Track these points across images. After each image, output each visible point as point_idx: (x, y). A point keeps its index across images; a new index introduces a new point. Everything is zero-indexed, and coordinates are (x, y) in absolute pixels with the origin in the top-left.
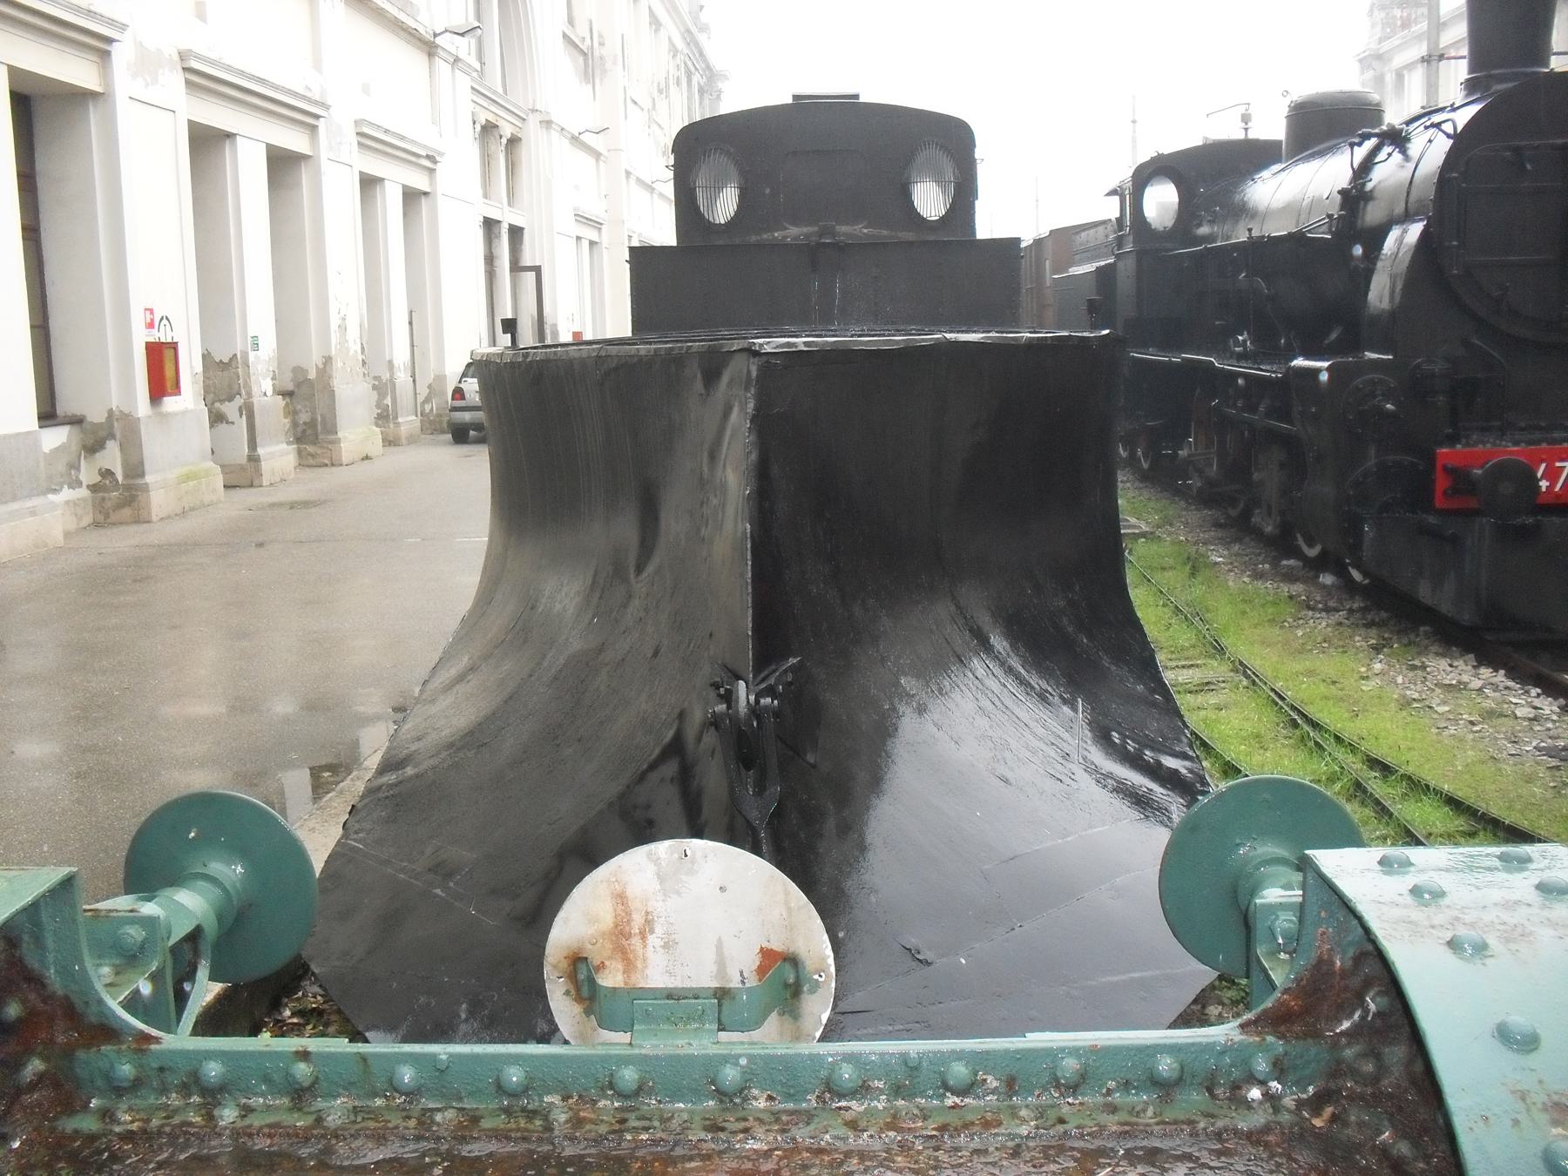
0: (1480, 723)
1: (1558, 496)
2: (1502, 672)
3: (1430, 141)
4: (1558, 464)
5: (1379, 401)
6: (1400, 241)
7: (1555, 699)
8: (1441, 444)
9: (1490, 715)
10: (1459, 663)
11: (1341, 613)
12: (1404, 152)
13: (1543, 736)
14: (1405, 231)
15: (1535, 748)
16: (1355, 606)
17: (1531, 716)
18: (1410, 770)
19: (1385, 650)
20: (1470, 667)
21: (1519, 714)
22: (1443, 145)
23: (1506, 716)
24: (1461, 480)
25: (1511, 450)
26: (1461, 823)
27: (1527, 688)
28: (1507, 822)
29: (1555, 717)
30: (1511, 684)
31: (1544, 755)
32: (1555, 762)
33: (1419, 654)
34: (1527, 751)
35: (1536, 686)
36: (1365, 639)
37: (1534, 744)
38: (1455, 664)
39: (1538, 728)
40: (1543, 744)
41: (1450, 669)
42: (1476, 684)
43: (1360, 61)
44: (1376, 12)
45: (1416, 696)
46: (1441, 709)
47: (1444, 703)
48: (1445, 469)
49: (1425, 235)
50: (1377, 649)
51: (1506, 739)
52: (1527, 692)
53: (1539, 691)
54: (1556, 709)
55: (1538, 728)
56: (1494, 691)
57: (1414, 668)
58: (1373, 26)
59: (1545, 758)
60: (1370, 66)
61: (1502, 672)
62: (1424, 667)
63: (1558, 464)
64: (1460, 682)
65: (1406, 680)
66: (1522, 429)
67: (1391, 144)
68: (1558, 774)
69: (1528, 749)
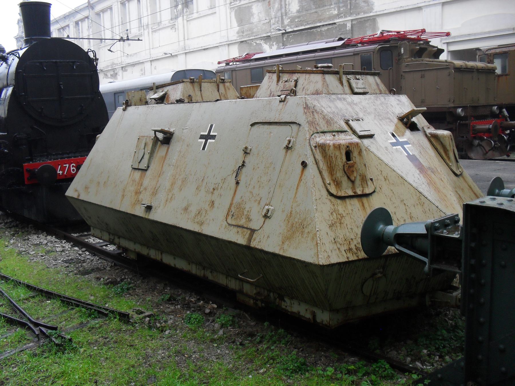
0: (45, 255)
1: (65, 176)
2: (54, 237)
3: (13, 59)
4: (64, 165)
5: (3, 149)
6: (6, 94)
7: (70, 243)
8: (25, 162)
9: (48, 252)
10: (41, 236)
11: (2, 224)
12: (7, 63)
13: (65, 257)
14: (7, 90)
15: (62, 261)
16: (8, 221)
17: (61, 250)
18: (15, 278)
19: (16, 235)
20: (44, 237)
21: (57, 250)
22: (17, 60)
23: (54, 252)
24: (32, 174)
25: (49, 162)
26: (31, 294)
27: (61, 241)
28: (45, 290)
29: (69, 249)
30: (57, 240)
31: (64, 263)
32: (67, 265)
33: (28, 234)
34: (59, 263)
35: (64, 239)
36: (9, 232)
37: (62, 260)
38: (39, 236)
39: (63, 254)
40: (65, 259)
41: (37, 238)
42: (45, 242)
43: (16, 39)
44: (20, 23)
45: (24, 250)
46: (32, 253)
47: (33, 251)
48: (27, 170)
49: (13, 91)
50: (13, 235)
51: (53, 260)
52: (62, 242)
53: (65, 241)
54: (70, 246)
55: (63, 254)
56: (51, 243)
57: (25, 240)
58: (20, 27)
59: (65, 264)
60: (20, 41)
61: (54, 237)
62: (28, 239)
63: (64, 165)
64: (40, 242)
65: (22, 244)
66: (54, 155)
67: (2, 61)
68: (68, 269)
69: (59, 262)
